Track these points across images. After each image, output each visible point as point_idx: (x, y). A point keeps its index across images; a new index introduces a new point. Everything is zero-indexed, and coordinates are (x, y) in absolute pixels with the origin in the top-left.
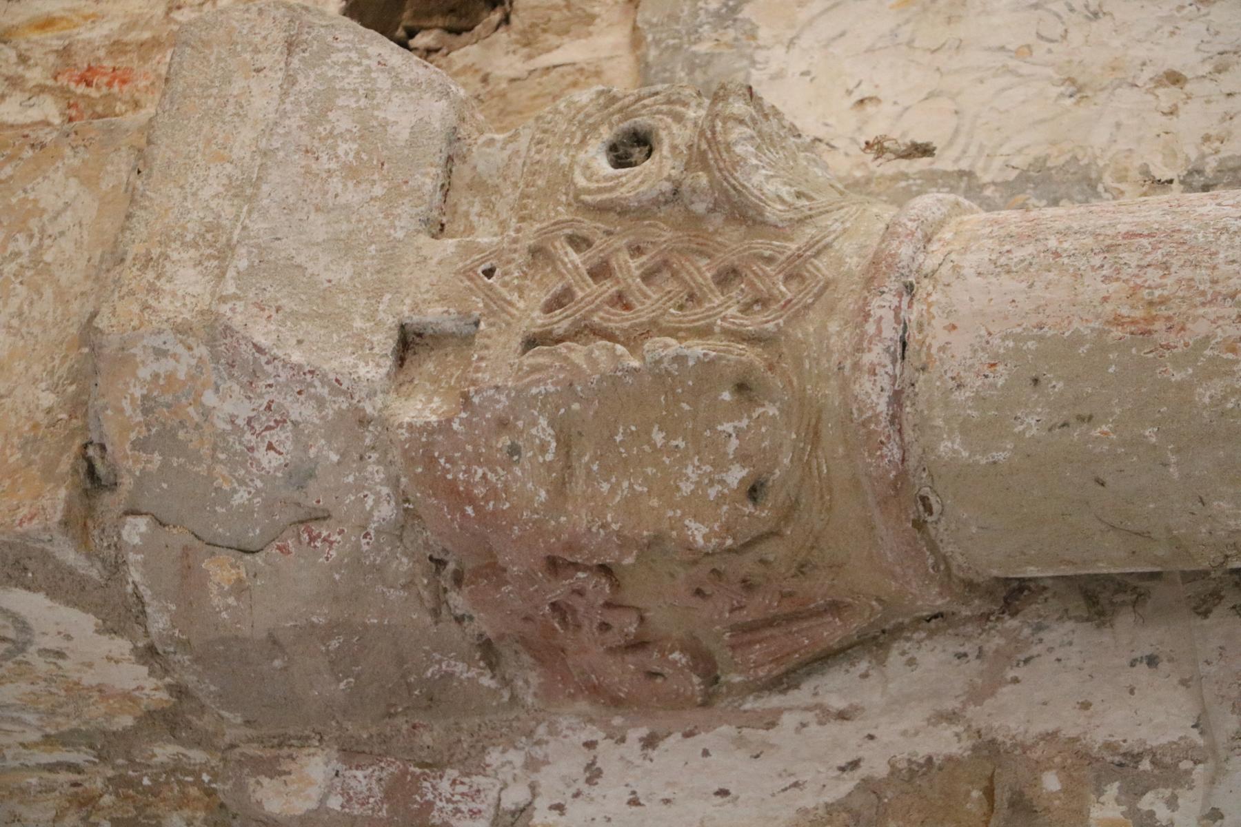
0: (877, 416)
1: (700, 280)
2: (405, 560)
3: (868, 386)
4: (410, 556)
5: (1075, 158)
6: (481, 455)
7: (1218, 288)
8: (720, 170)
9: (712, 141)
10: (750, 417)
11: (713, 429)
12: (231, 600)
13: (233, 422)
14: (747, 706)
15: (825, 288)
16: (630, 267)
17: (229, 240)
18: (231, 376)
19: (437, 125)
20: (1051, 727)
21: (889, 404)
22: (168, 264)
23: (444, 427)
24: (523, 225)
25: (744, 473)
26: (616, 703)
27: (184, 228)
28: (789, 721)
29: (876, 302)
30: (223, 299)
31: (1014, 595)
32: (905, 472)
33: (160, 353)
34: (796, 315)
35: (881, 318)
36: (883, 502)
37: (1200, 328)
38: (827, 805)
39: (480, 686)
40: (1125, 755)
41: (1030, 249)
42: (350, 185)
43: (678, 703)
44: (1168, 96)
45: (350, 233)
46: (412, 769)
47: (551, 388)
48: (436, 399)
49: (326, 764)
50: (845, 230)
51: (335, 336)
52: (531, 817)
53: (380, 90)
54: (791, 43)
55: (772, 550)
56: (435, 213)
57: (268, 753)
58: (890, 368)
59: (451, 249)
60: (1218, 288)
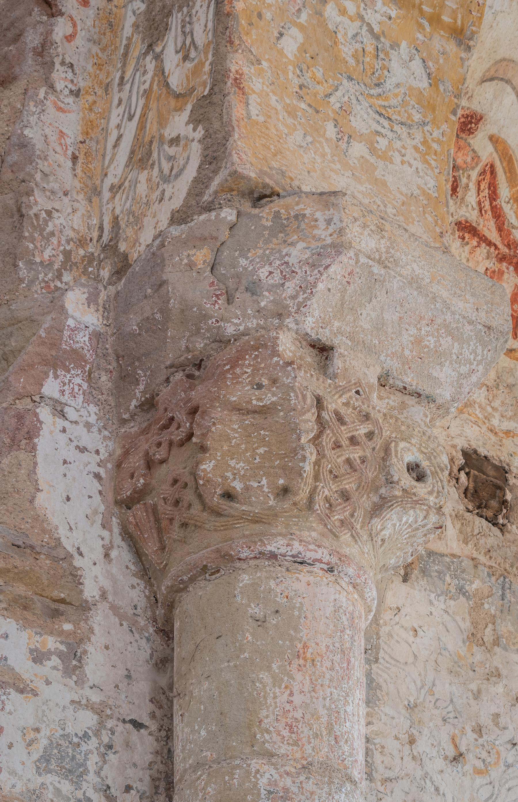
0: (265, 545)
1: (345, 482)
2: (202, 345)
3: (281, 542)
4: (204, 348)
5: (379, 700)
6: (258, 371)
7: (319, 686)
8: (402, 501)
9: (417, 502)
10: (269, 492)
11: (264, 475)
12: (186, 261)
13: (287, 255)
14: (114, 519)
15: (335, 536)
16: (356, 454)
17: (389, 268)
18: (313, 254)
19: (438, 391)
20: (96, 631)
21: (270, 551)
22: (379, 237)
23: (275, 353)
24: (381, 414)
25: (238, 489)
26: (119, 465)
27: (398, 250)
28: (106, 534)
29: (326, 552)
30: (356, 255)
31: (166, 632)
32: (233, 562)
33: (329, 222)
34: (321, 519)
35: (317, 552)
36: (218, 551)
37: (299, 676)
38: (59, 539)
39: (131, 401)
40: (81, 657)
41: (346, 623)
42: (412, 339)
43: (117, 490)
44: (405, 738)
45: (386, 333)
46: (88, 366)
47: (293, 402)
48: (291, 354)
49: (92, 324)
50: (363, 553)
51: (331, 310)
52: (60, 418)
53: (460, 367)
54: (446, 612)
55: (196, 509)
56: (391, 381)
57: (101, 301)
58: (289, 553)
59: (372, 381)
60: (319, 686)
